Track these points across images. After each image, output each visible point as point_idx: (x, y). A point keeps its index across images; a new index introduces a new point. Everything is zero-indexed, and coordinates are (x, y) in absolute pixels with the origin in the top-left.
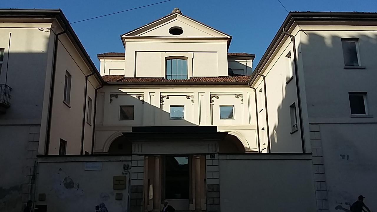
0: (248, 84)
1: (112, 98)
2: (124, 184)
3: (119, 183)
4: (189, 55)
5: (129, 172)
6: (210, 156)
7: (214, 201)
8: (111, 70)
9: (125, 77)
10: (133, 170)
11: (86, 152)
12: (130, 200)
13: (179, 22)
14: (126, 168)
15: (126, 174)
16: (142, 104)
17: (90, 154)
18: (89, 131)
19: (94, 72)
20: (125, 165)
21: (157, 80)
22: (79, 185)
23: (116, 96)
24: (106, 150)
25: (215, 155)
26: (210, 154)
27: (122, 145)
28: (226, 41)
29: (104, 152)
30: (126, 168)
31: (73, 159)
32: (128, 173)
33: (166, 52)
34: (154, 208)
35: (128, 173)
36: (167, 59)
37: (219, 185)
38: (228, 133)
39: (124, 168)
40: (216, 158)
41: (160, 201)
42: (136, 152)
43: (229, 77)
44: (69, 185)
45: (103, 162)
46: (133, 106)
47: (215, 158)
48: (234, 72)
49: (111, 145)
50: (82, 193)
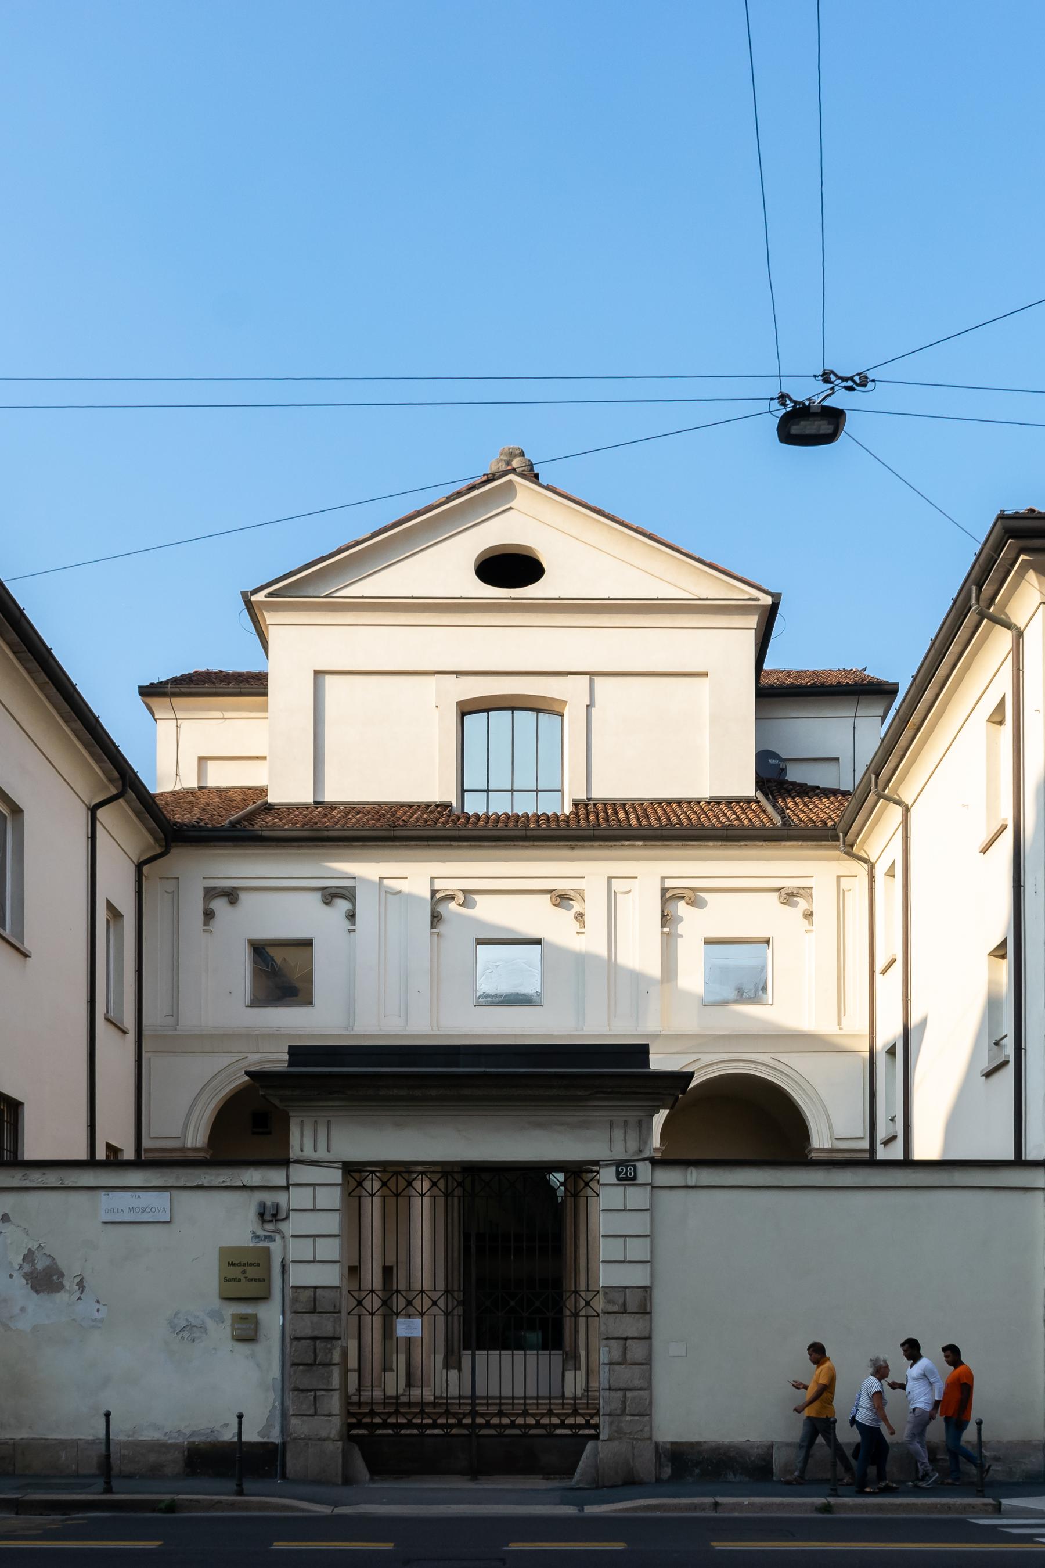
0: (835, 835)
1: (211, 906)
2: (263, 1280)
3: (246, 1277)
4: (571, 692)
5: (279, 1232)
6: (618, 1173)
7: (625, 1349)
8: (211, 764)
9: (271, 799)
10: (295, 1224)
11: (109, 1146)
12: (288, 1340)
13: (523, 521)
14: (267, 1217)
15: (270, 1238)
16: (350, 931)
17: (129, 1154)
18: (116, 1054)
19: (124, 785)
20: (263, 1206)
21: (418, 820)
22: (82, 1279)
23: (231, 896)
24: (197, 1137)
25: (635, 1166)
26: (619, 1164)
27: (254, 1122)
28: (753, 621)
29: (189, 1145)
30: (270, 1215)
31: (52, 1178)
32: (278, 1237)
33: (458, 673)
34: (409, 1385)
35: (278, 1237)
36: (466, 710)
37: (647, 1290)
38: (690, 1076)
39: (261, 1215)
40: (639, 1181)
41: (440, 1358)
42: (309, 1153)
43: (758, 802)
44: (45, 1280)
45: (175, 1192)
46: (308, 944)
47: (635, 1178)
48: (795, 774)
49: (219, 1113)
50: (98, 1311)
